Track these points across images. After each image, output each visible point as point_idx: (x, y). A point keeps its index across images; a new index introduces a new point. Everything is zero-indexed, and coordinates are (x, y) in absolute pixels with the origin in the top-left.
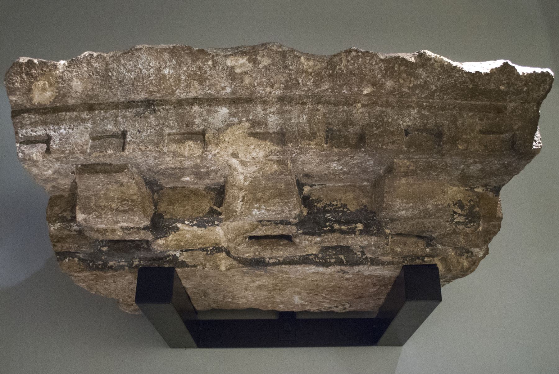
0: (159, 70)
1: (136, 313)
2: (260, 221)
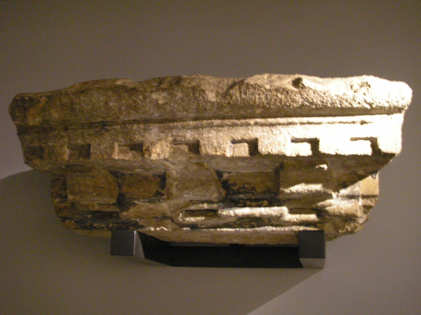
0: (106, 103)
1: (235, 121)
2: (191, 201)
